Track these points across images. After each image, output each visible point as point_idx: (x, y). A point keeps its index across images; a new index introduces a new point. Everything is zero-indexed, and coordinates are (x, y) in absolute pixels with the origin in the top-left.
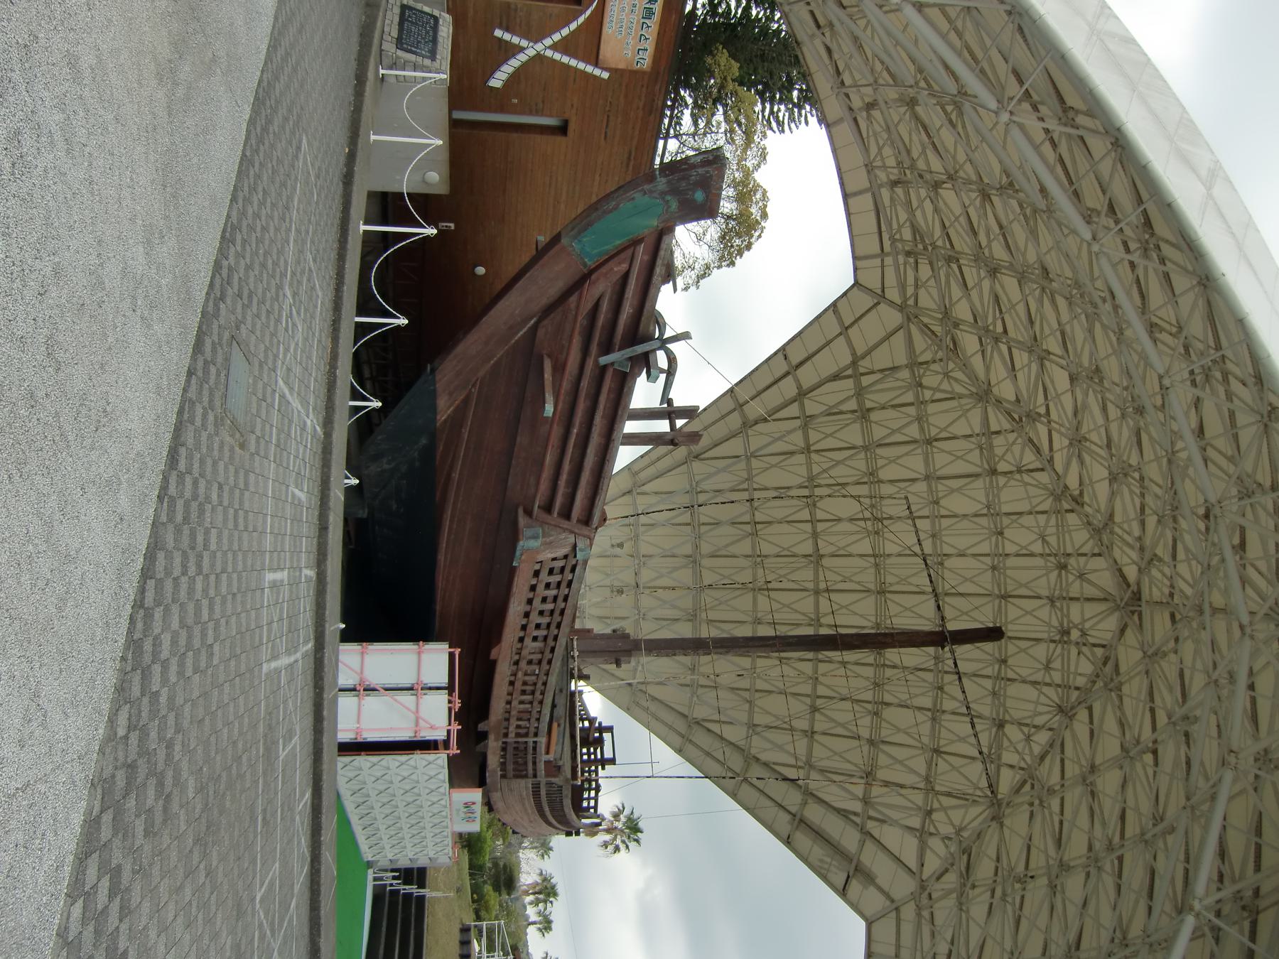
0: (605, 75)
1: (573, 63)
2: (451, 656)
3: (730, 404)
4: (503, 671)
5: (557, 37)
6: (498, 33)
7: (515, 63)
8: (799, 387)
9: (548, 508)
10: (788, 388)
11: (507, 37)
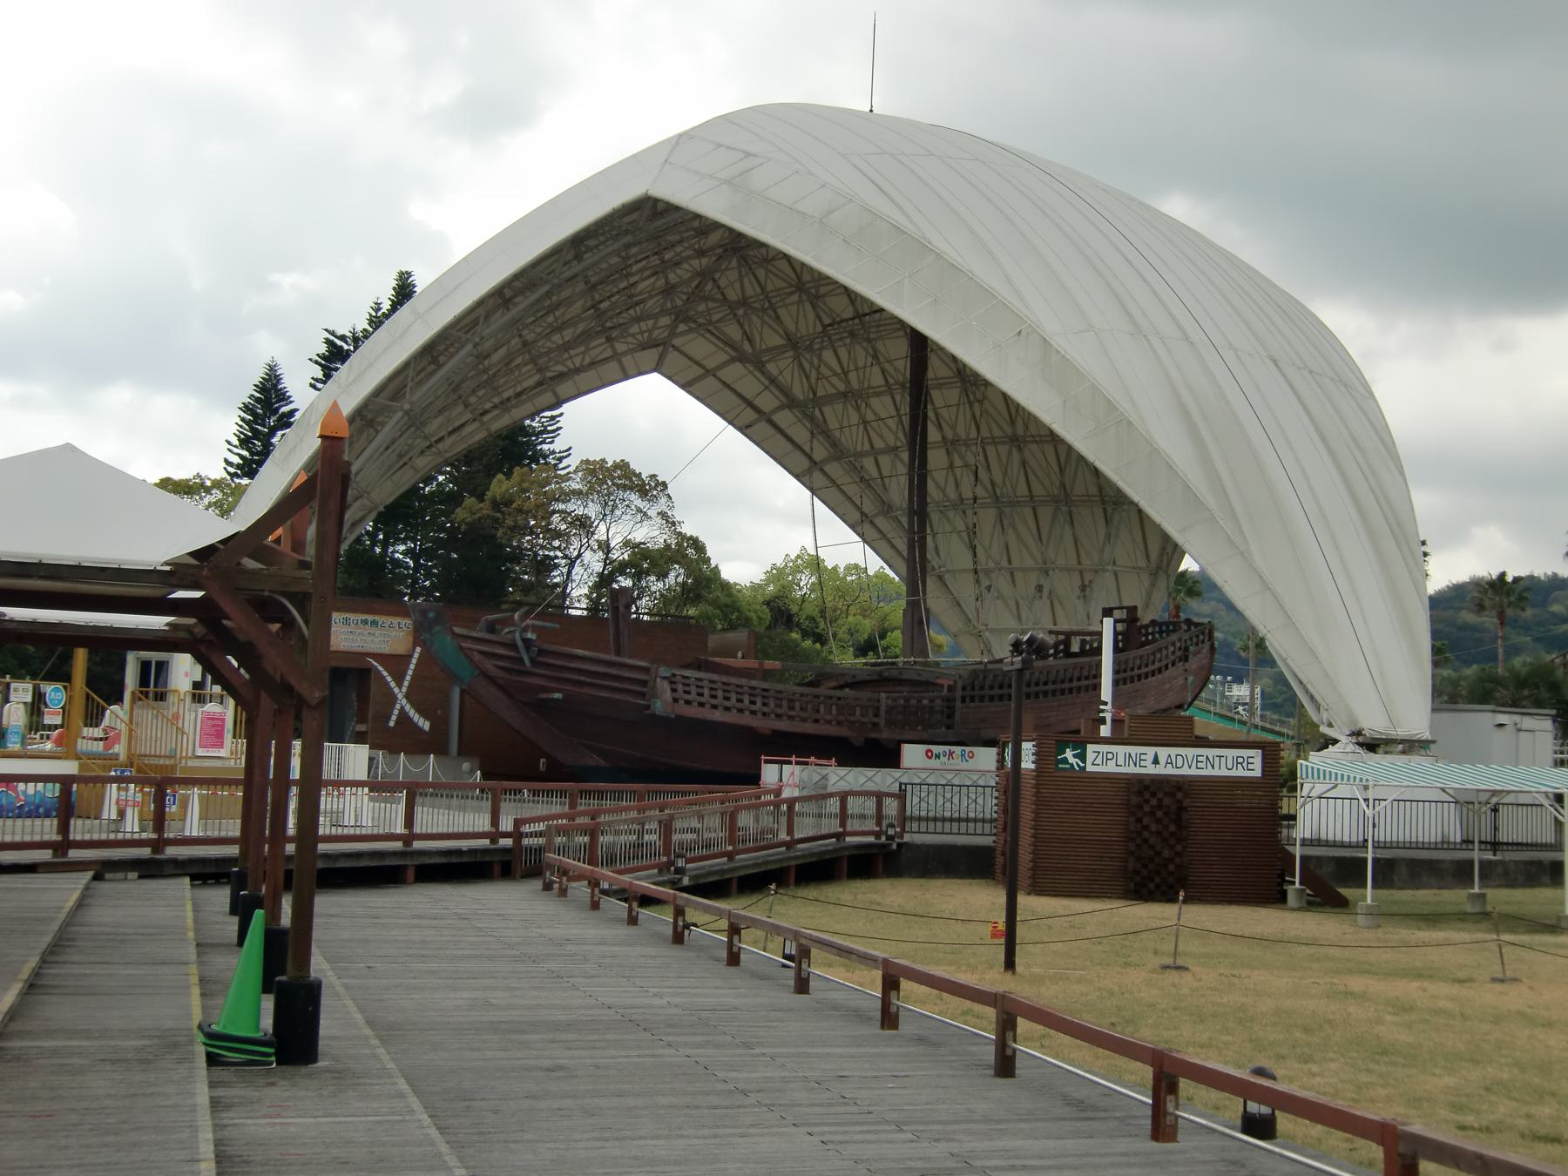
0: (418, 649)
1: (410, 672)
2: (767, 762)
3: (818, 478)
4: (783, 725)
5: (393, 684)
6: (392, 724)
7: (412, 713)
8: (782, 407)
9: (642, 695)
10: (785, 418)
11: (394, 718)
